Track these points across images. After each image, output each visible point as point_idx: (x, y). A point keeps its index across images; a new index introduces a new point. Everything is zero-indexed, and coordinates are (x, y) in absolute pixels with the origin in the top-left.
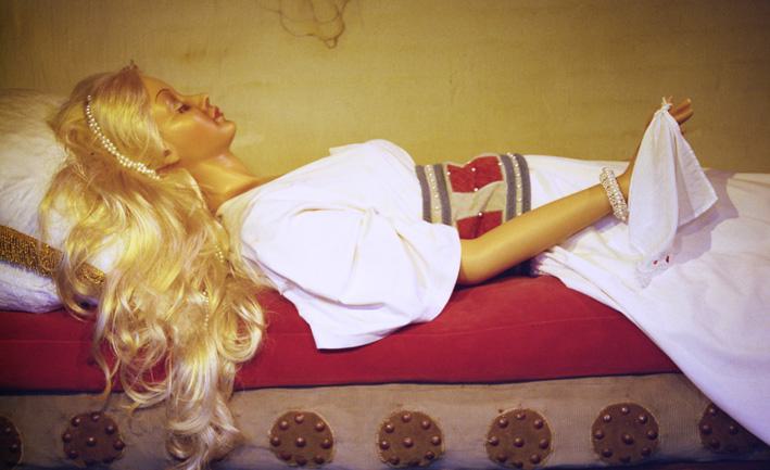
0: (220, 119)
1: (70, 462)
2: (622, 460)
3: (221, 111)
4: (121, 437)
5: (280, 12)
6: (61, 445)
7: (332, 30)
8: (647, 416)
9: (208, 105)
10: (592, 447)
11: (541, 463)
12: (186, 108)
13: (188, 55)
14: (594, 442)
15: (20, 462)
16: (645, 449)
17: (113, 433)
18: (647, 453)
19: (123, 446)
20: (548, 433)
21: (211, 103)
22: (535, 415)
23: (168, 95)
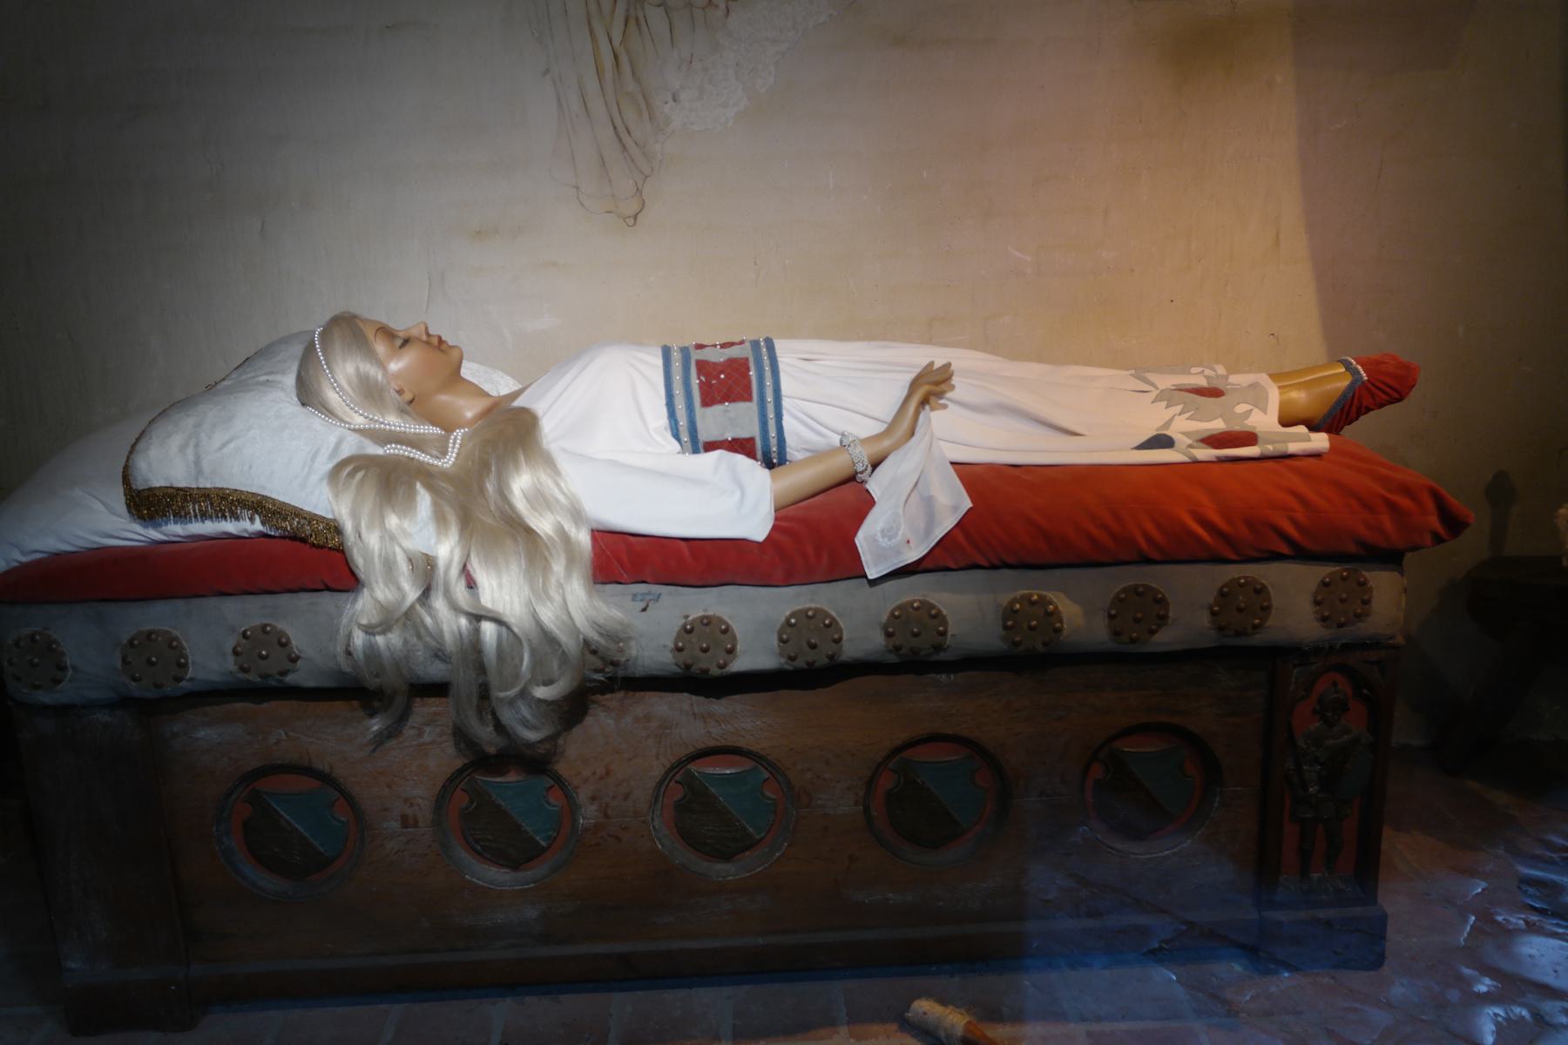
0: (444, 347)
1: (241, 676)
2: (808, 664)
3: (444, 339)
4: (295, 650)
5: (577, 188)
6: (231, 659)
7: (632, 207)
8: (833, 621)
9: (428, 335)
10: (778, 651)
11: (727, 669)
12: (406, 342)
13: (478, 233)
14: (779, 646)
15: (188, 676)
16: (830, 653)
17: (284, 644)
18: (831, 657)
19: (298, 658)
20: (734, 638)
21: (431, 332)
22: (721, 621)
23: (387, 333)
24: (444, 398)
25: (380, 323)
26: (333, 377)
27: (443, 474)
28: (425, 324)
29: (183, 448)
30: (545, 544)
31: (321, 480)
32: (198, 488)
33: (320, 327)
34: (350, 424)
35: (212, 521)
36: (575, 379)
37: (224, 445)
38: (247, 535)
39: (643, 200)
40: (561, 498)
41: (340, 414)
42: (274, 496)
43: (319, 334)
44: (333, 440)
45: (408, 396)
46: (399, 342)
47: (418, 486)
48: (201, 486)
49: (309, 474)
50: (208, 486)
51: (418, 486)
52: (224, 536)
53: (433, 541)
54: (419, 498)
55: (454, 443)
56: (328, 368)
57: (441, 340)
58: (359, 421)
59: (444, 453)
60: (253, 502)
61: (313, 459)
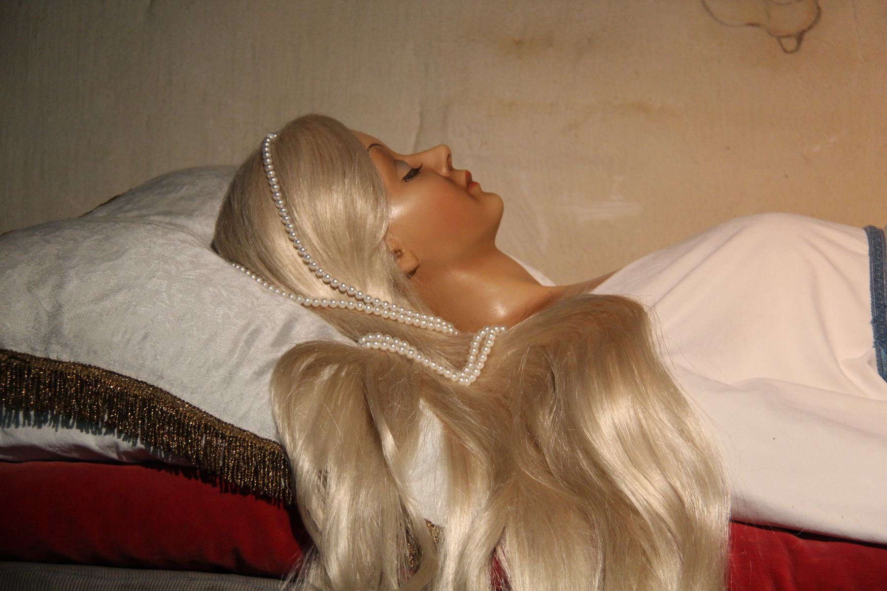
3: (474, 179)
9: (450, 168)
12: (414, 173)
13: (518, 43)
21: (455, 166)
24: (463, 277)
25: (374, 139)
26: (288, 214)
27: (462, 393)
28: (448, 149)
29: (31, 287)
30: (644, 528)
31: (260, 373)
32: (47, 360)
33: (274, 134)
34: (305, 297)
35: (55, 426)
36: (708, 257)
37: (105, 296)
38: (114, 456)
39: (819, 8)
40: (686, 451)
41: (291, 278)
42: (175, 391)
43: (272, 143)
44: (280, 318)
45: (408, 263)
46: (404, 172)
47: (422, 403)
48: (53, 357)
49: (238, 365)
50: (65, 358)
51: (422, 403)
52: (75, 455)
53: (440, 502)
54: (423, 423)
55: (482, 346)
56: (284, 197)
57: (470, 183)
58: (322, 292)
59: (459, 366)
60: (136, 396)
61: (249, 343)
